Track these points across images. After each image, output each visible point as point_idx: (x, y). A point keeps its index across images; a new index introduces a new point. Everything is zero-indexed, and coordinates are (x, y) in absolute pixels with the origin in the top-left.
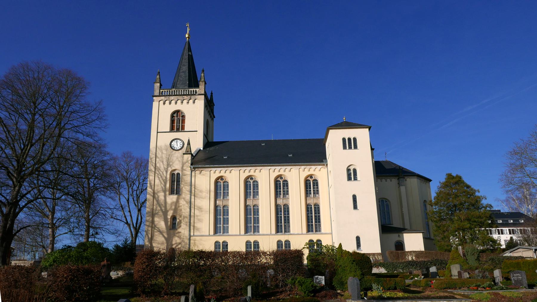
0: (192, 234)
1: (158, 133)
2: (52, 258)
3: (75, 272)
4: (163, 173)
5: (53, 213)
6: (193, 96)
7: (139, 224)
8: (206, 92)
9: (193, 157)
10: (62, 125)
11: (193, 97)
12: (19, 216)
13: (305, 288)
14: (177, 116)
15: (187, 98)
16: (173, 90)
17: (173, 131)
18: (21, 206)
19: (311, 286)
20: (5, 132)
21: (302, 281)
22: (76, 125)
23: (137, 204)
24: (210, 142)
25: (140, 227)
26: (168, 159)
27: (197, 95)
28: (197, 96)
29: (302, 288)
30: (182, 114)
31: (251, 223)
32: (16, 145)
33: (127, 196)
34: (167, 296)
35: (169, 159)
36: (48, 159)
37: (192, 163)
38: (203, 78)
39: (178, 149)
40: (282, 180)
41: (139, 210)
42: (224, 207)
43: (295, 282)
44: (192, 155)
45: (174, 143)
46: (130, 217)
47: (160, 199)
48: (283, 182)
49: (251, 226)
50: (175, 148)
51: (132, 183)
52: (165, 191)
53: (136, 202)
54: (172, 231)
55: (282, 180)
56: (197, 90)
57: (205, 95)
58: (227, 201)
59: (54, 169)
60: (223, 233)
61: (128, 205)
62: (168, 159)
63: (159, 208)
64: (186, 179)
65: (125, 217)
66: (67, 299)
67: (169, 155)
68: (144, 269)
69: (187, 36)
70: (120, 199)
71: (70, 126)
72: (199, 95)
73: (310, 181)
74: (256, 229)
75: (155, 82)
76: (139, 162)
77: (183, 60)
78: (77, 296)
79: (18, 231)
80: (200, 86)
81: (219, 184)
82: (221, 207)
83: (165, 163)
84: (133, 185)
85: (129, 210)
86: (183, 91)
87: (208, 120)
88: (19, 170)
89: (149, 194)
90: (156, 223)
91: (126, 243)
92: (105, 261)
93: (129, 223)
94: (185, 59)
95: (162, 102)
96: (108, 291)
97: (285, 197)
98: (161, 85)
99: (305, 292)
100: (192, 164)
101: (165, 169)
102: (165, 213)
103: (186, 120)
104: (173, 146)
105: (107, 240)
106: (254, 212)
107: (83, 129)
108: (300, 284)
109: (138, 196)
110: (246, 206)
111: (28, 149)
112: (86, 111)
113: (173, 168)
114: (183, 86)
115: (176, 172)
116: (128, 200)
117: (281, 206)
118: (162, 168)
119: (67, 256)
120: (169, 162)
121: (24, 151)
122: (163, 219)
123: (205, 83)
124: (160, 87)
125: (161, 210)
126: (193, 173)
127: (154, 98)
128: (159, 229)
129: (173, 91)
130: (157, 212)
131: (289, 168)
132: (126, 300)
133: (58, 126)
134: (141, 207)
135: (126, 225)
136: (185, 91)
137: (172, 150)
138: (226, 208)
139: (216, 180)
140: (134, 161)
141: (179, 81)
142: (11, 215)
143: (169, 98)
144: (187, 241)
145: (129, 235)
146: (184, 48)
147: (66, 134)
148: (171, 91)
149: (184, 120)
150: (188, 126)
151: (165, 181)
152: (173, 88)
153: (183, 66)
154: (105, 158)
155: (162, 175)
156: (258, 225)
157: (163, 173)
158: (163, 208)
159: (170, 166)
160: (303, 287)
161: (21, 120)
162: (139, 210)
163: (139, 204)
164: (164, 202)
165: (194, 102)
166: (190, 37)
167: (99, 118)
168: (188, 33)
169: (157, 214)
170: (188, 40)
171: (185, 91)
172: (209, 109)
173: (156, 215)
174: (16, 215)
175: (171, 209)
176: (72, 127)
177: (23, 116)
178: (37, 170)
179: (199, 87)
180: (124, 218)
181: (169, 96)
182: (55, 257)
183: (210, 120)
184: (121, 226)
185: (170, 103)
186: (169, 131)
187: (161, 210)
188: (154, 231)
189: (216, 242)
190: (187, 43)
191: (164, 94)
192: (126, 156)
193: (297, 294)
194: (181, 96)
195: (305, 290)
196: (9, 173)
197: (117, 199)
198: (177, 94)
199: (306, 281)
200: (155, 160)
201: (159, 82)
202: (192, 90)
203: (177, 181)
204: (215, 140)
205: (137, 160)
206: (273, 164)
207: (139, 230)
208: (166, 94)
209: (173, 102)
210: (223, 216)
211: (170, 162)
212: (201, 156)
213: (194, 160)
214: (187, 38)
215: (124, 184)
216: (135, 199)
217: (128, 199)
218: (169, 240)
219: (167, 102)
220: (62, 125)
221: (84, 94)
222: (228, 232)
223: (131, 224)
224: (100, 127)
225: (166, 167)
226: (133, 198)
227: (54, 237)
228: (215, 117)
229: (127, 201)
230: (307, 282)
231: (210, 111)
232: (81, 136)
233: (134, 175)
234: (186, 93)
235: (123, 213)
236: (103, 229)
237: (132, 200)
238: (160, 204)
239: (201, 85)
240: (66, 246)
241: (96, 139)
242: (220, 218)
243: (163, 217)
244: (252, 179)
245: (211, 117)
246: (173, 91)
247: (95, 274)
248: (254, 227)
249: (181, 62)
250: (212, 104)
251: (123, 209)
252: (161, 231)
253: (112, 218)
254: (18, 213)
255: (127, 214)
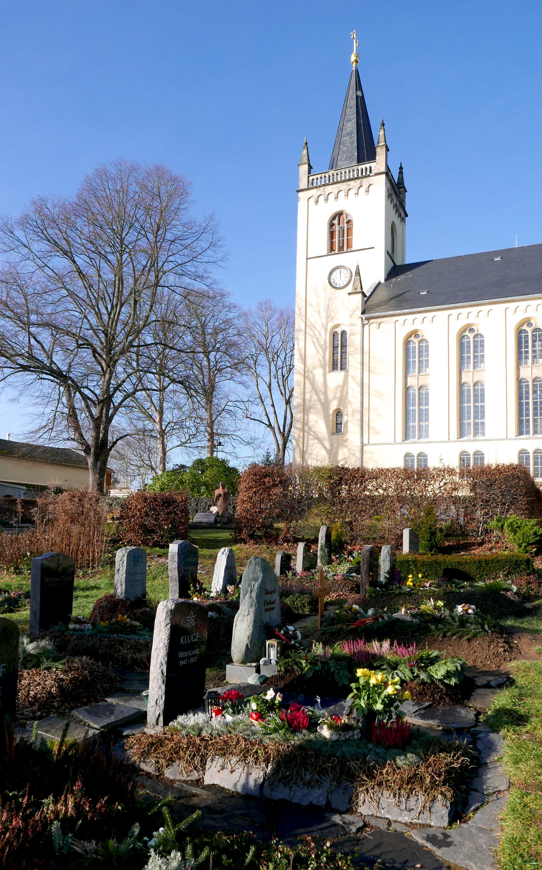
0: (365, 441)
1: (308, 260)
2: (158, 484)
3: (152, 501)
4: (319, 332)
5: (161, 413)
6: (365, 179)
7: (288, 426)
8: (388, 167)
9: (366, 298)
10: (160, 265)
11: (366, 182)
12: (113, 421)
13: (521, 538)
14: (339, 224)
15: (355, 184)
16: (331, 173)
17: (333, 252)
18: (116, 404)
19: (534, 535)
20: (86, 288)
21: (517, 523)
22: (180, 262)
23: (283, 393)
24: (399, 266)
25: (289, 431)
26: (328, 306)
27: (372, 176)
28: (372, 178)
29: (515, 537)
30: (347, 218)
31: (469, 418)
32: (101, 306)
33: (267, 379)
34: (288, 544)
35: (330, 306)
36: (145, 326)
37: (365, 310)
38: (383, 139)
39: (342, 285)
40: (531, 328)
41: (288, 402)
42: (420, 388)
43: (502, 526)
44: (364, 295)
45: (335, 275)
46: (273, 415)
47: (316, 381)
48: (533, 332)
49: (469, 424)
50: (336, 284)
51: (276, 356)
52: (323, 367)
53: (282, 387)
54: (335, 437)
55: (531, 328)
56: (373, 165)
57: (388, 173)
58: (426, 377)
59: (158, 342)
60: (419, 438)
61: (269, 395)
62: (328, 306)
63: (315, 397)
64: (354, 341)
65: (267, 415)
66: (142, 543)
67: (330, 299)
68: (251, 498)
69: (353, 58)
70: (257, 385)
71: (172, 265)
72: (377, 174)
73: (527, 332)
74: (423, 433)
75: (300, 163)
76: (285, 316)
77: (348, 110)
78: (156, 539)
79: (115, 443)
80: (377, 157)
81: (466, 340)
82: (415, 390)
83: (323, 314)
84: (276, 359)
85: (271, 403)
86: (347, 172)
87: (393, 224)
88: (109, 348)
89: (299, 373)
90: (311, 423)
91: (267, 460)
92: (221, 487)
93: (273, 425)
94: (351, 107)
95: (312, 201)
96: (215, 535)
97: (537, 363)
98: (310, 167)
99: (520, 546)
100: (363, 313)
101: (323, 327)
102: (325, 405)
103: (354, 228)
104: (334, 282)
105: (240, 455)
106: (475, 396)
107: (190, 268)
108: (512, 529)
109: (285, 377)
110: (407, 389)
111: (117, 312)
112: (192, 235)
113: (336, 322)
114: (348, 162)
115: (339, 330)
116: (269, 387)
117: (528, 382)
118: (319, 326)
119: (179, 481)
120: (329, 313)
121: (112, 316)
122: (322, 416)
123: (387, 150)
124: (309, 172)
125: (319, 400)
126: (366, 327)
127: (300, 194)
128: (317, 435)
129: (331, 175)
130: (312, 403)
131: (430, 315)
132: (183, 541)
133: (153, 268)
134: (290, 397)
135: (269, 429)
136: (351, 171)
137: (334, 290)
138: (423, 391)
139: (459, 334)
140: (277, 316)
141: (341, 153)
142: (104, 419)
143: (324, 191)
144: (358, 454)
145: (274, 446)
146: (349, 85)
147: (171, 279)
148: (327, 176)
149: (351, 228)
150: (357, 242)
151: (324, 347)
152: (332, 169)
153: (347, 122)
154: (231, 315)
155: (319, 337)
156: (482, 421)
157: (319, 332)
158: (322, 397)
159: (332, 319)
160: (518, 535)
161: (106, 265)
162: (288, 402)
163: (287, 392)
164: (323, 385)
165: (367, 191)
166: (358, 60)
167: (212, 245)
168: (355, 52)
169: (311, 407)
170: (356, 67)
171: (351, 171)
172: (395, 200)
173: (312, 411)
174: (109, 420)
175: (334, 398)
176: (175, 266)
177: (106, 257)
178: (131, 345)
179: (375, 159)
180: (266, 417)
181: (324, 187)
182: (162, 483)
183: (397, 221)
184: (261, 431)
185: (326, 200)
186: (326, 254)
187: (319, 400)
188: (308, 438)
189: (407, 455)
190: (354, 73)
191: (315, 185)
192: (263, 308)
193: (507, 548)
194: (345, 183)
195: (521, 542)
196: (94, 351)
197: (253, 385)
198: (337, 180)
199: (523, 524)
200: (304, 311)
201: (307, 161)
202: (363, 167)
203: (342, 346)
204: (408, 261)
205: (282, 314)
206: (514, 298)
207: (288, 437)
208: (319, 184)
209: (332, 197)
210: (419, 405)
211: (331, 313)
212: (382, 294)
213: (368, 303)
214: (354, 63)
215: (262, 359)
216: (281, 384)
217: (270, 384)
218: (332, 452)
219: (322, 199)
220: (160, 265)
221: (186, 205)
222: (427, 436)
223: (276, 427)
224: (214, 260)
225: (324, 321)
226: (278, 382)
227: (164, 453)
228: (407, 216)
229: (269, 387)
230: (527, 526)
231: (398, 203)
232: (186, 280)
233: (276, 342)
234: (353, 175)
235: (262, 408)
236: (234, 437)
237: (277, 385)
238: (318, 389)
239: (379, 155)
240: (177, 465)
241: (209, 281)
242: (467, 407)
243: (322, 413)
244: (471, 330)
245: (400, 215)
246: (331, 175)
247: (178, 506)
248: (476, 424)
249: (343, 114)
250: (401, 190)
251: (262, 402)
252: (320, 437)
253: (247, 417)
254: (112, 416)
255: (270, 410)
